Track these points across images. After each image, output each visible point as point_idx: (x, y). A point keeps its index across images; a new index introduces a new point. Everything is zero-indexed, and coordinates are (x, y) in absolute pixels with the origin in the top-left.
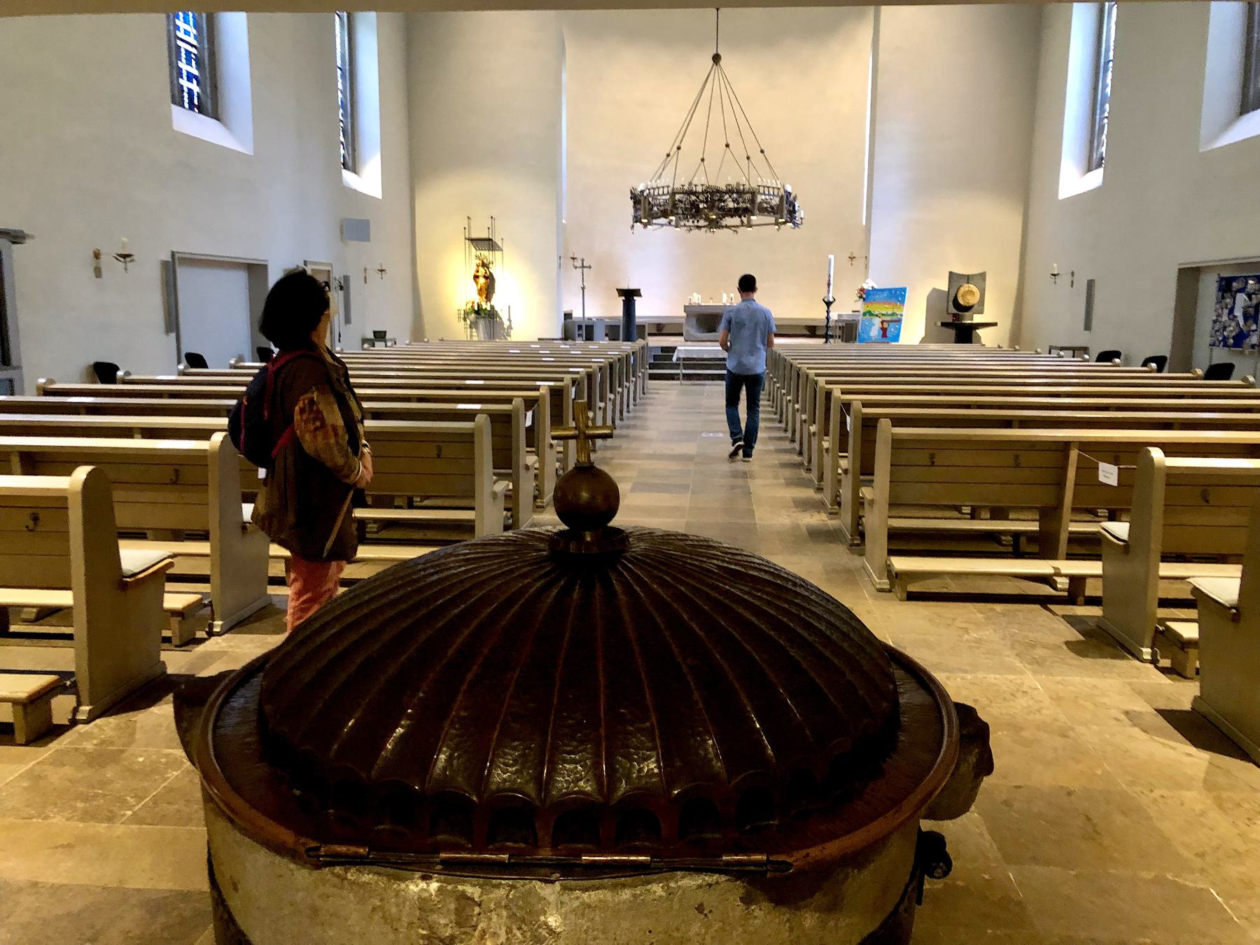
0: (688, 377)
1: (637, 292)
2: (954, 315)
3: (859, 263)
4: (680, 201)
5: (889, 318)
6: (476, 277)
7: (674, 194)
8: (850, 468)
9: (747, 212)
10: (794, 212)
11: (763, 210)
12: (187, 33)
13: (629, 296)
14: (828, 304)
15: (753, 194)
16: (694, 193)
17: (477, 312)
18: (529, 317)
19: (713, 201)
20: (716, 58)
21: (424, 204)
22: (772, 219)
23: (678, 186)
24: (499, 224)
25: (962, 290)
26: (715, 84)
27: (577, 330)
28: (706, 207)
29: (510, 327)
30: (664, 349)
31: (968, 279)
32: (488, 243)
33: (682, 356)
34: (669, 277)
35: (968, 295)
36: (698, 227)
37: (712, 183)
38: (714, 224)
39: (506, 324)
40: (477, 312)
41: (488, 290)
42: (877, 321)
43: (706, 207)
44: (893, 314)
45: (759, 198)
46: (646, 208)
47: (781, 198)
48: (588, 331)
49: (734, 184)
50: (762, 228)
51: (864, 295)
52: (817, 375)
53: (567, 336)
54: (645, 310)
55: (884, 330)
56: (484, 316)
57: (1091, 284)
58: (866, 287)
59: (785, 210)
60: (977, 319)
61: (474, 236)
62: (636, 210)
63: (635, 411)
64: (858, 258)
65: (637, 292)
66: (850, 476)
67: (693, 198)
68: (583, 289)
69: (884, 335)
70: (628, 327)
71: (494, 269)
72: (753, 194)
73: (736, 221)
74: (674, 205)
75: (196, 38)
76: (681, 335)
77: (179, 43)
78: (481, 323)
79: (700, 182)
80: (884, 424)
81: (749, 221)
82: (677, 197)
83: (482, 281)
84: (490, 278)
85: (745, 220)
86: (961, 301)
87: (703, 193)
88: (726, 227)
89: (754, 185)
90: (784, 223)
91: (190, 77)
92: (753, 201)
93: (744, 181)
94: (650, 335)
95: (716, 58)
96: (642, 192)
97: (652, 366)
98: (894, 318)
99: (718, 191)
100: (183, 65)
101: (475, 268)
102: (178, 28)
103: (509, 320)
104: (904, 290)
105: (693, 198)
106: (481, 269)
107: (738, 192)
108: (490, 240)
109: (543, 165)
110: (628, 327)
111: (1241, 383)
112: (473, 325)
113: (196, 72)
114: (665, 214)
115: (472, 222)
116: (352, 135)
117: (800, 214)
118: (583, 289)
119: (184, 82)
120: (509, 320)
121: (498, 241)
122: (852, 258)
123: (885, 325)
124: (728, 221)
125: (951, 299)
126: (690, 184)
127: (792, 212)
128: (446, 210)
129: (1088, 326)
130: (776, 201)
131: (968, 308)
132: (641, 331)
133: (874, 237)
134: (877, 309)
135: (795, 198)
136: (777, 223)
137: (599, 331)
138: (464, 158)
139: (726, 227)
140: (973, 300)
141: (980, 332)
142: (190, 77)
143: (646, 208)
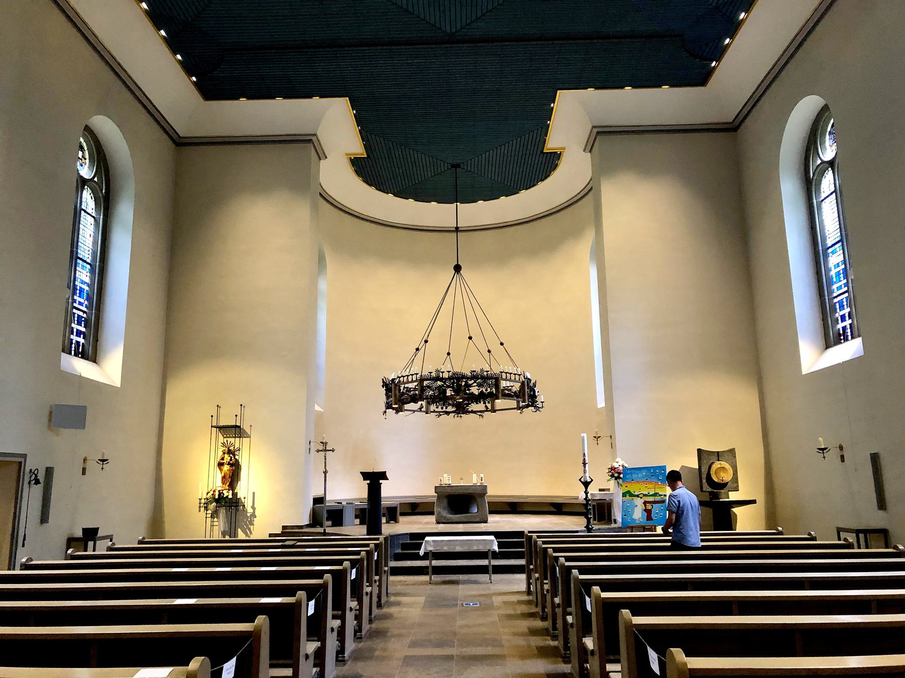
0: (438, 570)
1: (383, 475)
2: (710, 493)
3: (604, 442)
4: (428, 387)
5: (651, 499)
6: (220, 465)
7: (422, 380)
8: (596, 649)
9: (493, 397)
10: (536, 397)
11: (507, 394)
12: (80, 303)
13: (374, 479)
14: (586, 484)
15: (497, 379)
16: (441, 379)
17: (217, 501)
18: (272, 504)
19: (459, 386)
20: (458, 268)
21: (177, 391)
22: (513, 403)
23: (425, 373)
24: (247, 412)
25: (714, 467)
26: (456, 295)
27: (326, 514)
28: (454, 394)
29: (254, 515)
30: (413, 536)
31: (718, 455)
32: (236, 430)
33: (430, 548)
34: (415, 458)
35: (722, 472)
36: (448, 413)
37: (457, 369)
38: (461, 410)
39: (250, 510)
40: (217, 501)
41: (233, 477)
42: (639, 502)
43: (454, 394)
44: (655, 495)
45: (503, 384)
46: (397, 396)
47: (523, 383)
48: (336, 516)
49: (478, 370)
50: (506, 416)
51: (616, 474)
52: (556, 550)
53: (315, 520)
54: (390, 491)
55: (648, 512)
56: (227, 504)
57: (875, 459)
58: (616, 465)
59: (527, 396)
60: (733, 496)
61: (222, 423)
62: (388, 397)
63: (358, 656)
64: (605, 437)
65: (383, 475)
66: (575, 629)
67: (439, 383)
68: (325, 473)
69: (649, 518)
70: (373, 512)
71: (243, 459)
72: (497, 379)
73: (480, 406)
74: (423, 389)
75: (86, 307)
76: (432, 513)
77: (74, 311)
78: (222, 512)
79: (447, 369)
80: (575, 572)
81: (493, 406)
82: (425, 383)
83: (226, 468)
84: (236, 467)
85: (489, 406)
86: (715, 479)
87: (449, 378)
88: (473, 412)
89: (496, 370)
90: (527, 406)
91: (79, 333)
92: (497, 385)
93: (487, 368)
94: (403, 514)
95: (458, 268)
96: (393, 380)
97: (398, 557)
98: (658, 498)
99: (463, 377)
100: (75, 326)
101: (220, 454)
102: (74, 301)
103: (253, 507)
104: (98, 529)
105: (439, 383)
106: (226, 456)
107: (482, 378)
108: (236, 427)
109: (299, 356)
110: (373, 512)
111: (807, 536)
112: (215, 514)
113: (83, 329)
114: (414, 399)
115: (222, 411)
116: (94, 325)
117: (540, 398)
118: (325, 473)
119: (74, 338)
120: (253, 507)
121: (246, 427)
122: (597, 438)
123: (649, 507)
124: (474, 407)
125: (704, 476)
126: (437, 371)
127: (533, 397)
128: (197, 396)
129: (882, 504)
130: (516, 387)
131: (723, 486)
132: (393, 514)
133: (618, 417)
134: (635, 489)
135: (535, 385)
136: (519, 408)
137: (349, 516)
138: (216, 350)
139: (473, 412)
140: (727, 477)
141: (736, 510)
142: (79, 333)
143: (397, 396)
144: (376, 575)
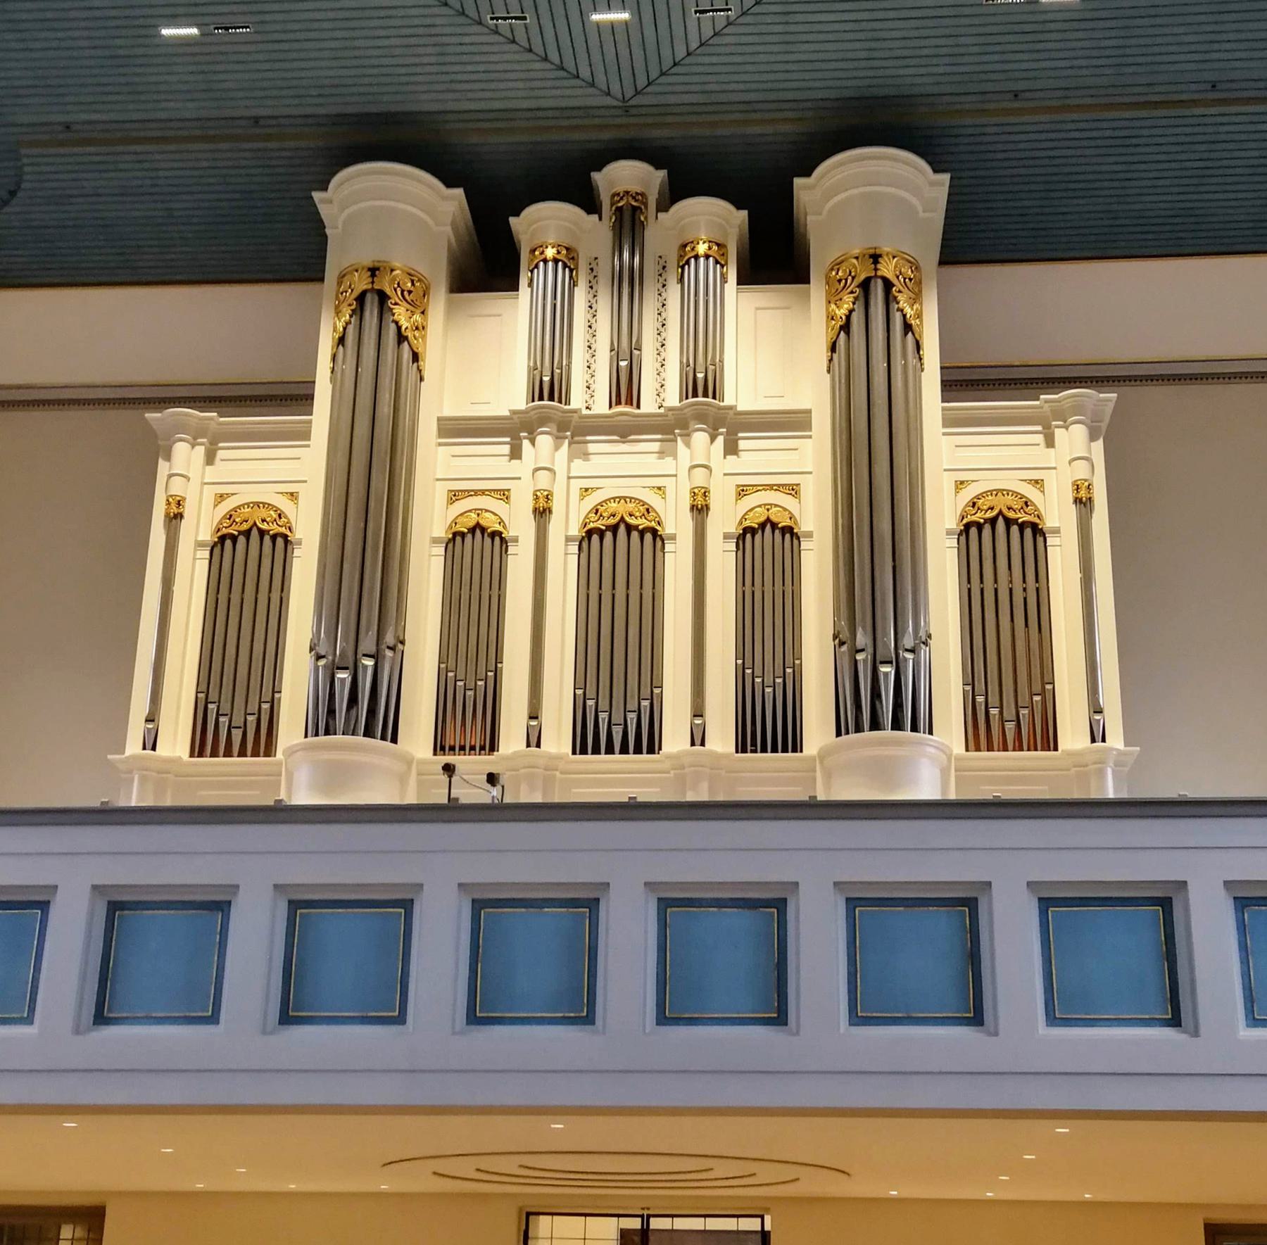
144: (1004, 538)
